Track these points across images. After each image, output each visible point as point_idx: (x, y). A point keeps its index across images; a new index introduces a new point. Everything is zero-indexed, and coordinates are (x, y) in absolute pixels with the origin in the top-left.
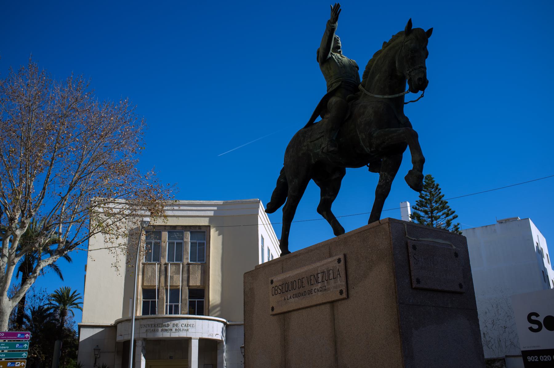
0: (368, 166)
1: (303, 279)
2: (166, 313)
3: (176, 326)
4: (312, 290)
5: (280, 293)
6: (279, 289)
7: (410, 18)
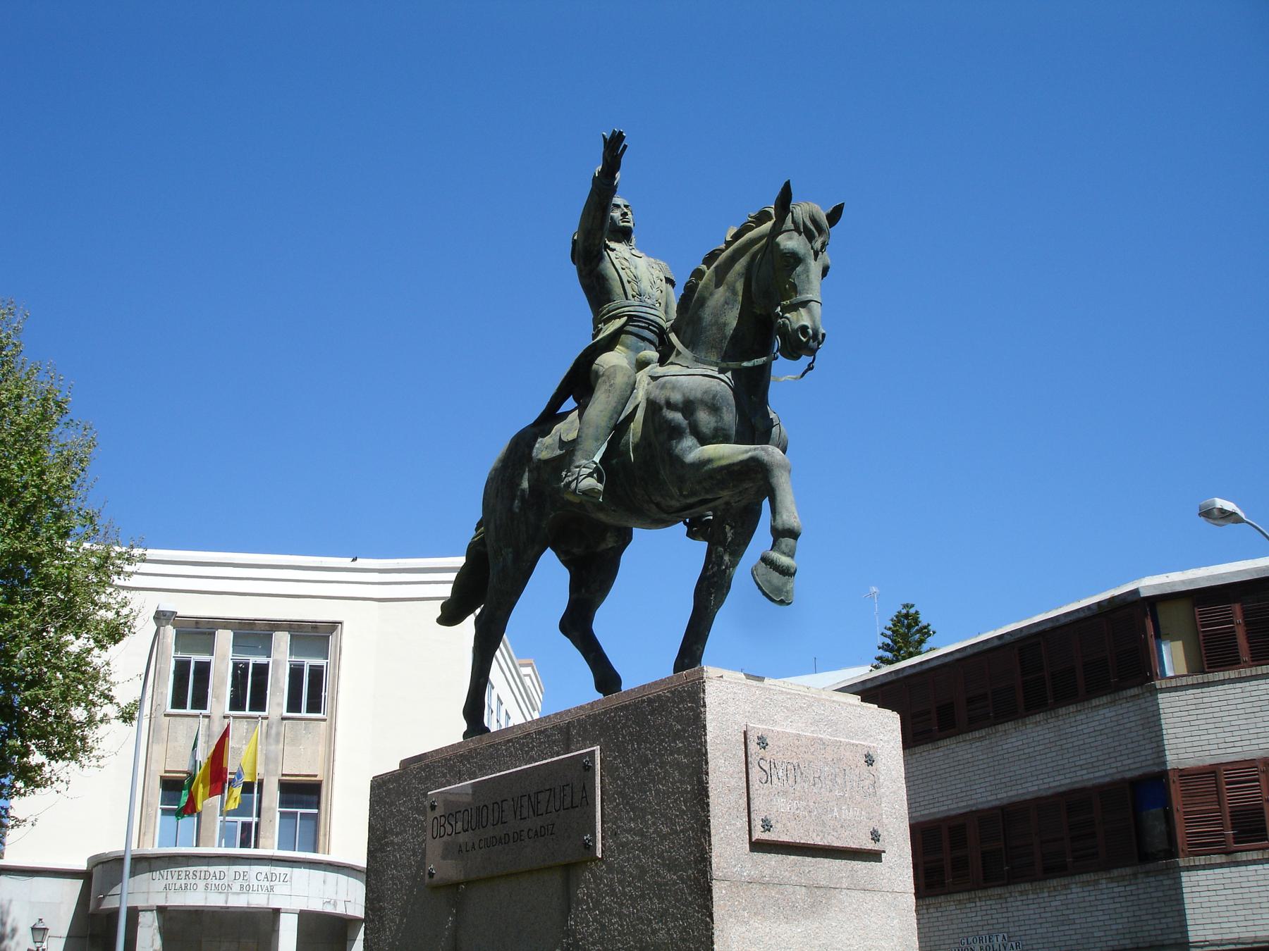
0: (685, 523)
1: (504, 803)
2: (220, 846)
3: (242, 878)
4: (523, 831)
5: (450, 835)
6: (449, 823)
7: (786, 180)
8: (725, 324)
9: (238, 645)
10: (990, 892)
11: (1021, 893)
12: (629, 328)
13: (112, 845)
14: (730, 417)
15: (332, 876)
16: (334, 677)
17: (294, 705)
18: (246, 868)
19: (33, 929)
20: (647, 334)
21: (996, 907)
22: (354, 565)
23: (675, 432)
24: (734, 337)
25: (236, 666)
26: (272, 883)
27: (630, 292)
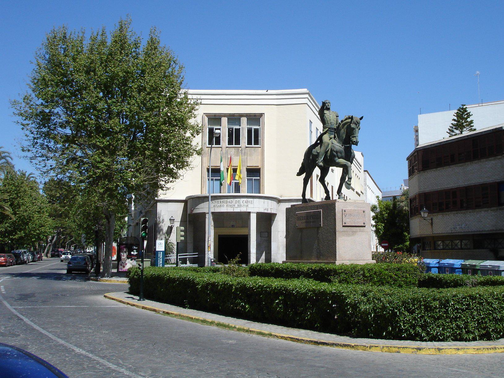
8: (343, 137)
9: (229, 122)
10: (462, 211)
11: (470, 212)
12: (329, 130)
13: (196, 192)
14: (343, 154)
15: (266, 201)
16: (263, 132)
17: (249, 142)
18: (239, 199)
19: (170, 219)
20: (332, 130)
21: (463, 216)
22: (267, 93)
23: (335, 156)
24: (344, 139)
25: (229, 129)
26: (248, 204)
27: (329, 123)
